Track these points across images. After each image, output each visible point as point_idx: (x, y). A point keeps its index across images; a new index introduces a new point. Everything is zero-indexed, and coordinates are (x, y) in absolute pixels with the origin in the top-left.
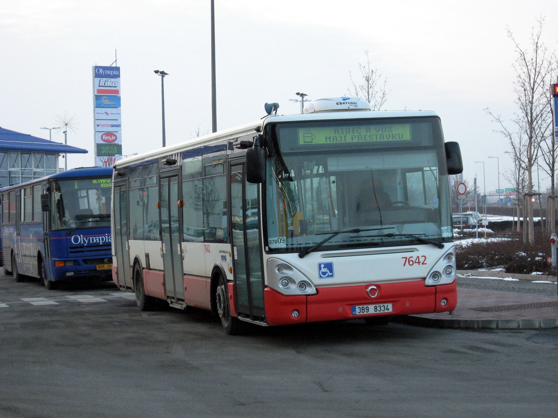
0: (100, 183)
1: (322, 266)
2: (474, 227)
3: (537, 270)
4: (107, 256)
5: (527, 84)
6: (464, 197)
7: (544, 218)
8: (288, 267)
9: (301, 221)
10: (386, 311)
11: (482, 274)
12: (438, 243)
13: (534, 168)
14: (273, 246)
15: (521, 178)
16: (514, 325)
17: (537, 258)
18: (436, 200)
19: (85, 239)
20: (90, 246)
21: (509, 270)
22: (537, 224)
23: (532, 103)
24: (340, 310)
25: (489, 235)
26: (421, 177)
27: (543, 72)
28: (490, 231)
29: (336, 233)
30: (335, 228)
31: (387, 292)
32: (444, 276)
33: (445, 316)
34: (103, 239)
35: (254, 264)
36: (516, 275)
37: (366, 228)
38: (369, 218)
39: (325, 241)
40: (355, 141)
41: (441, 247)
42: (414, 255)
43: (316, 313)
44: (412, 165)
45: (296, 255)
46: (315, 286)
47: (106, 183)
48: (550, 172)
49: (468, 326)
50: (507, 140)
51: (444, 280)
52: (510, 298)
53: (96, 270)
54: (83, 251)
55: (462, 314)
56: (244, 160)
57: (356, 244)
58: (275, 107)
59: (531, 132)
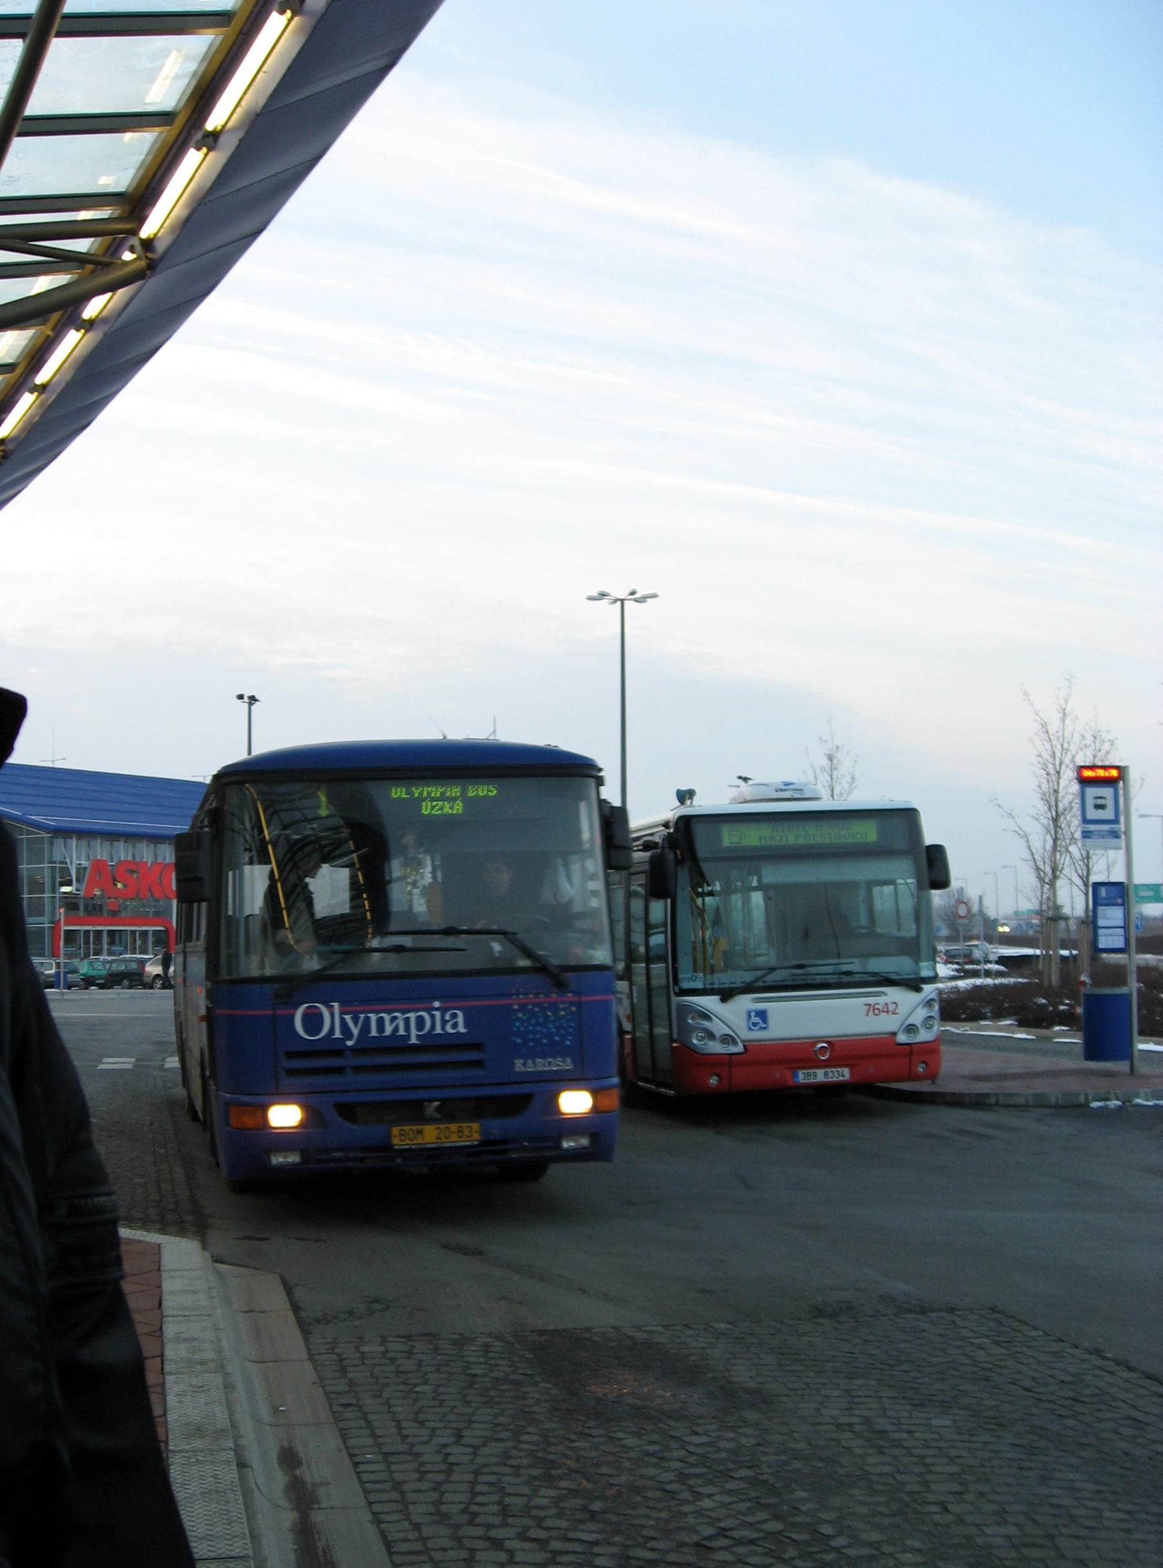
0: (421, 799)
1: (753, 1014)
2: (978, 962)
3: (1061, 1024)
4: (437, 1094)
5: (1050, 766)
6: (965, 921)
7: (1074, 952)
8: (706, 1016)
9: (725, 952)
10: (841, 1078)
11: (986, 1028)
12: (914, 984)
13: (1059, 883)
14: (685, 985)
15: (1045, 896)
16: (1020, 1100)
17: (1062, 1007)
18: (914, 926)
19: (348, 1018)
20: (366, 1047)
21: (1023, 1024)
22: (1064, 959)
23: (1056, 791)
24: (777, 1075)
25: (999, 974)
26: (893, 891)
27: (1073, 748)
28: (1002, 968)
29: (772, 970)
30: (773, 962)
31: (843, 1051)
32: (922, 1031)
33: (925, 1086)
34: (420, 1022)
35: (660, 1009)
36: (1032, 1030)
37: (820, 962)
38: (821, 946)
39: (757, 980)
40: (801, 841)
41: (918, 990)
42: (881, 1000)
43: (743, 1078)
44: (882, 876)
45: (716, 998)
46: (743, 1041)
47: (443, 798)
48: (1083, 888)
49: (956, 1101)
50: (1023, 842)
51: (924, 1036)
52: (1019, 1063)
53: (388, 1147)
54: (339, 1070)
55: (948, 1085)
56: (646, 867)
57: (802, 983)
58: (690, 794)
59: (1056, 832)
